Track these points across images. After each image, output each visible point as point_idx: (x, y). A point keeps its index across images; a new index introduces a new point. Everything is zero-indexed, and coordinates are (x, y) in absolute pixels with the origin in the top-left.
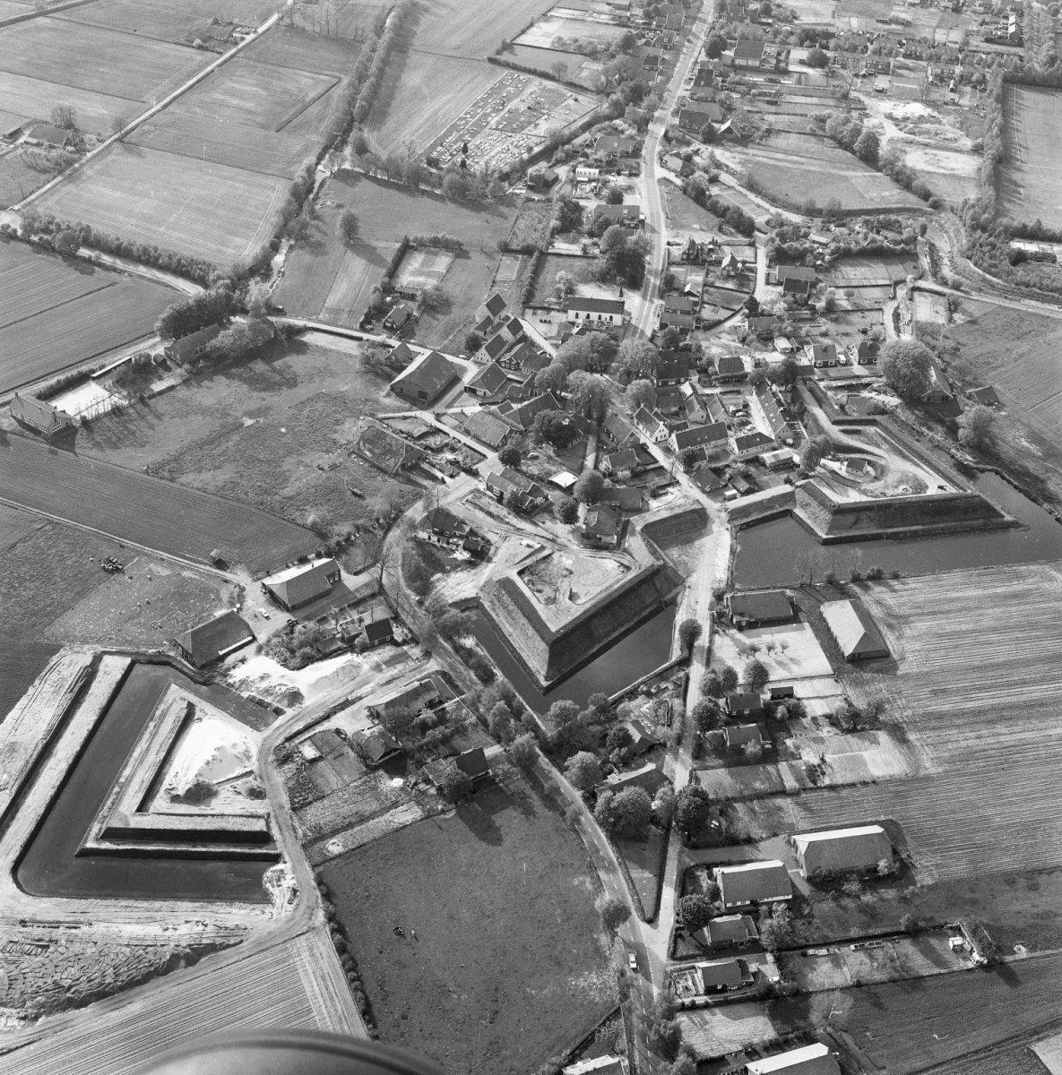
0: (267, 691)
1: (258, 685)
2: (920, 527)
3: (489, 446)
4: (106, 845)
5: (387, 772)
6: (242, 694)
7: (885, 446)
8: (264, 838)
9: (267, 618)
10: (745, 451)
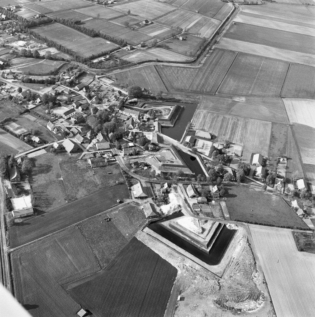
0: (174, 209)
1: (171, 210)
2: (178, 116)
3: (109, 149)
4: (210, 248)
5: (210, 202)
6: (170, 214)
7: (152, 107)
8: (220, 225)
9: (148, 201)
10: (68, 116)
